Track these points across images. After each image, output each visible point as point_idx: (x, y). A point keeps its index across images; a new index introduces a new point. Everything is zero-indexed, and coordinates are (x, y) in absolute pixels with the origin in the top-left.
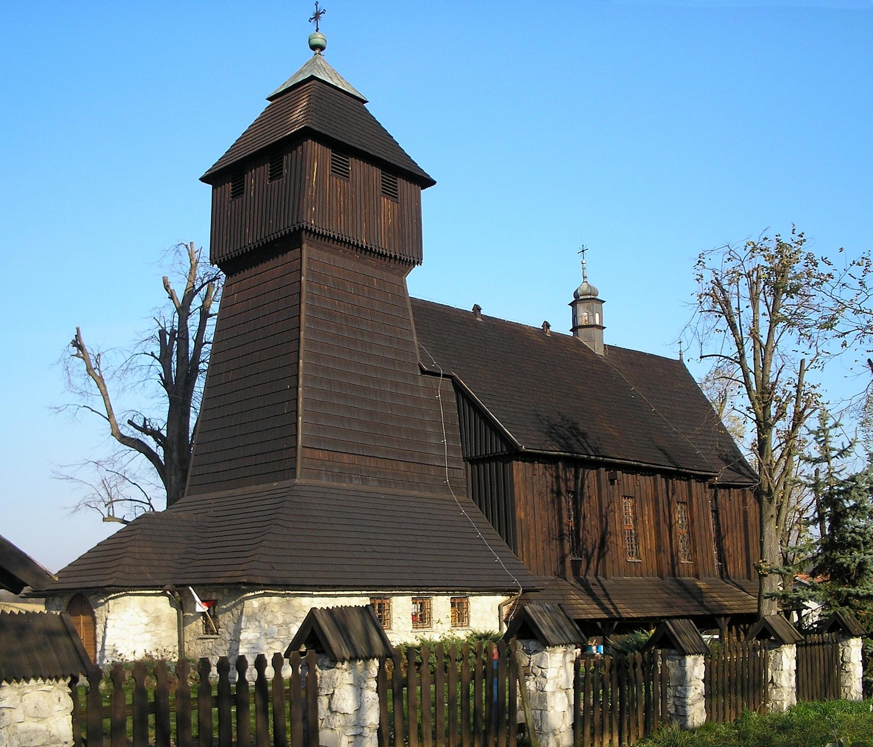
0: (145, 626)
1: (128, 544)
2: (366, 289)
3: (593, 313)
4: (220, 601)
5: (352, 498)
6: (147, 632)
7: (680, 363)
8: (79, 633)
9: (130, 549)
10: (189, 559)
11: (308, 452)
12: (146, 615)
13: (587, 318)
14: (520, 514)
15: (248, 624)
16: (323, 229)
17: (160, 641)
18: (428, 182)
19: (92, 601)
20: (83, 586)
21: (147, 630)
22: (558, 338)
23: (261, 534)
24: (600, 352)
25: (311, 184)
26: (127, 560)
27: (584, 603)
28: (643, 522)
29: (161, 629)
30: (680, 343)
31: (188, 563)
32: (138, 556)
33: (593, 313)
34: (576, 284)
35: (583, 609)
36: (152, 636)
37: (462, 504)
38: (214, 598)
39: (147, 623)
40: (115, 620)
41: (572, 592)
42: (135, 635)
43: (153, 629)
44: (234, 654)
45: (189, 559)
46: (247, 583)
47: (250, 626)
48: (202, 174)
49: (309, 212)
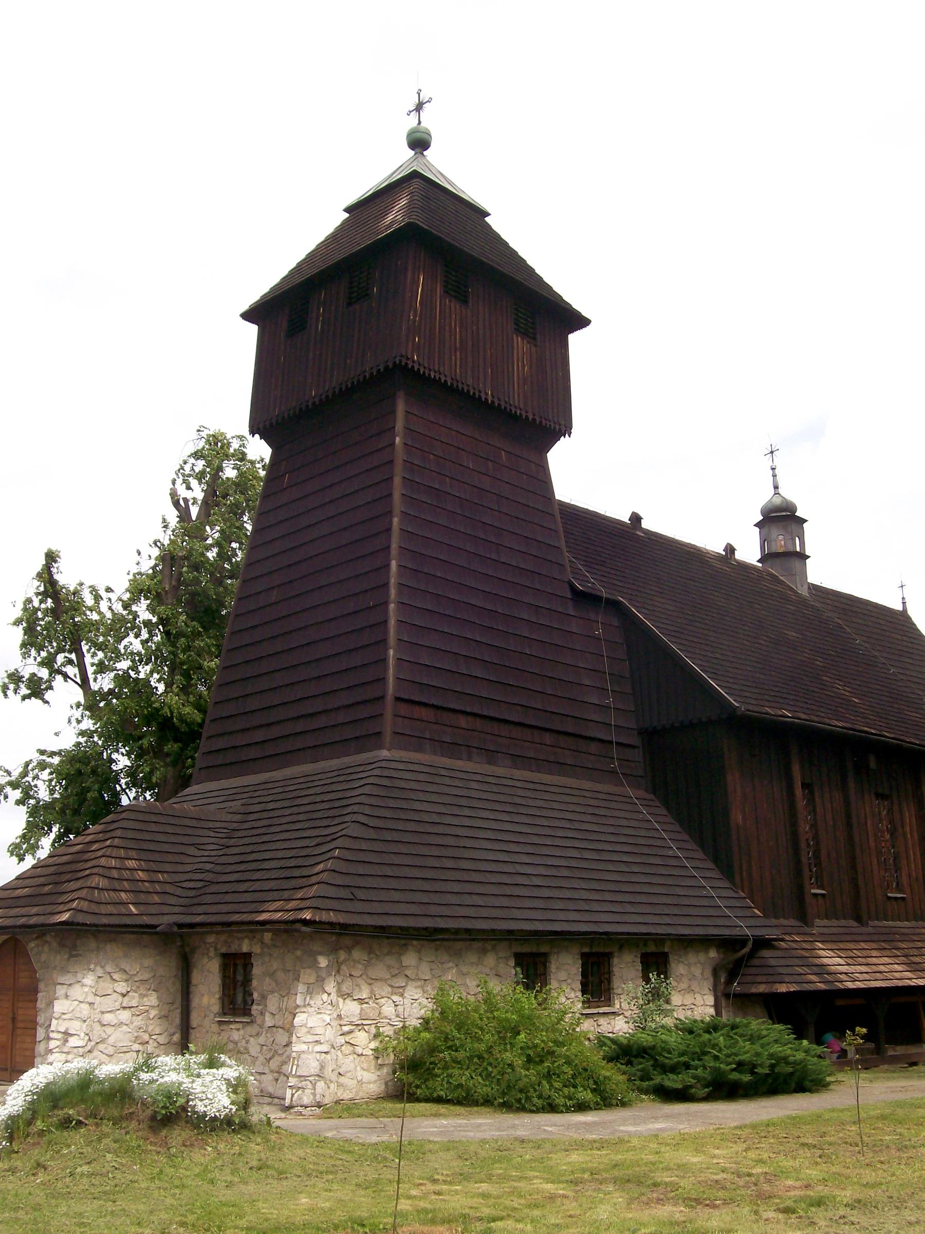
0: (120, 998)
1: (100, 853)
2: (490, 464)
3: (792, 535)
4: (256, 954)
5: (474, 785)
6: (124, 1008)
7: (904, 614)
8: (599, 594)
9: (103, 862)
10: (201, 880)
11: (404, 709)
12: (125, 977)
13: (783, 542)
14: (737, 817)
15: (308, 998)
16: (430, 370)
17: (147, 1026)
18: (580, 322)
19: (32, 949)
20: (18, 924)
21: (124, 1005)
22: (744, 567)
23: (329, 839)
24: (804, 592)
25: (414, 304)
26: (96, 881)
27: (845, 963)
28: (904, 834)
29: (149, 1004)
30: (902, 586)
31: (200, 888)
32: (115, 874)
33: (792, 535)
34: (764, 496)
35: (846, 973)
36: (133, 1015)
37: (629, 800)
38: (245, 949)
39: (124, 992)
40: (70, 985)
41: (820, 945)
42: (103, 1013)
43: (134, 1003)
44: (280, 1052)
45: (201, 880)
46: (310, 920)
47: (312, 1002)
48: (245, 307)
49: (410, 344)
